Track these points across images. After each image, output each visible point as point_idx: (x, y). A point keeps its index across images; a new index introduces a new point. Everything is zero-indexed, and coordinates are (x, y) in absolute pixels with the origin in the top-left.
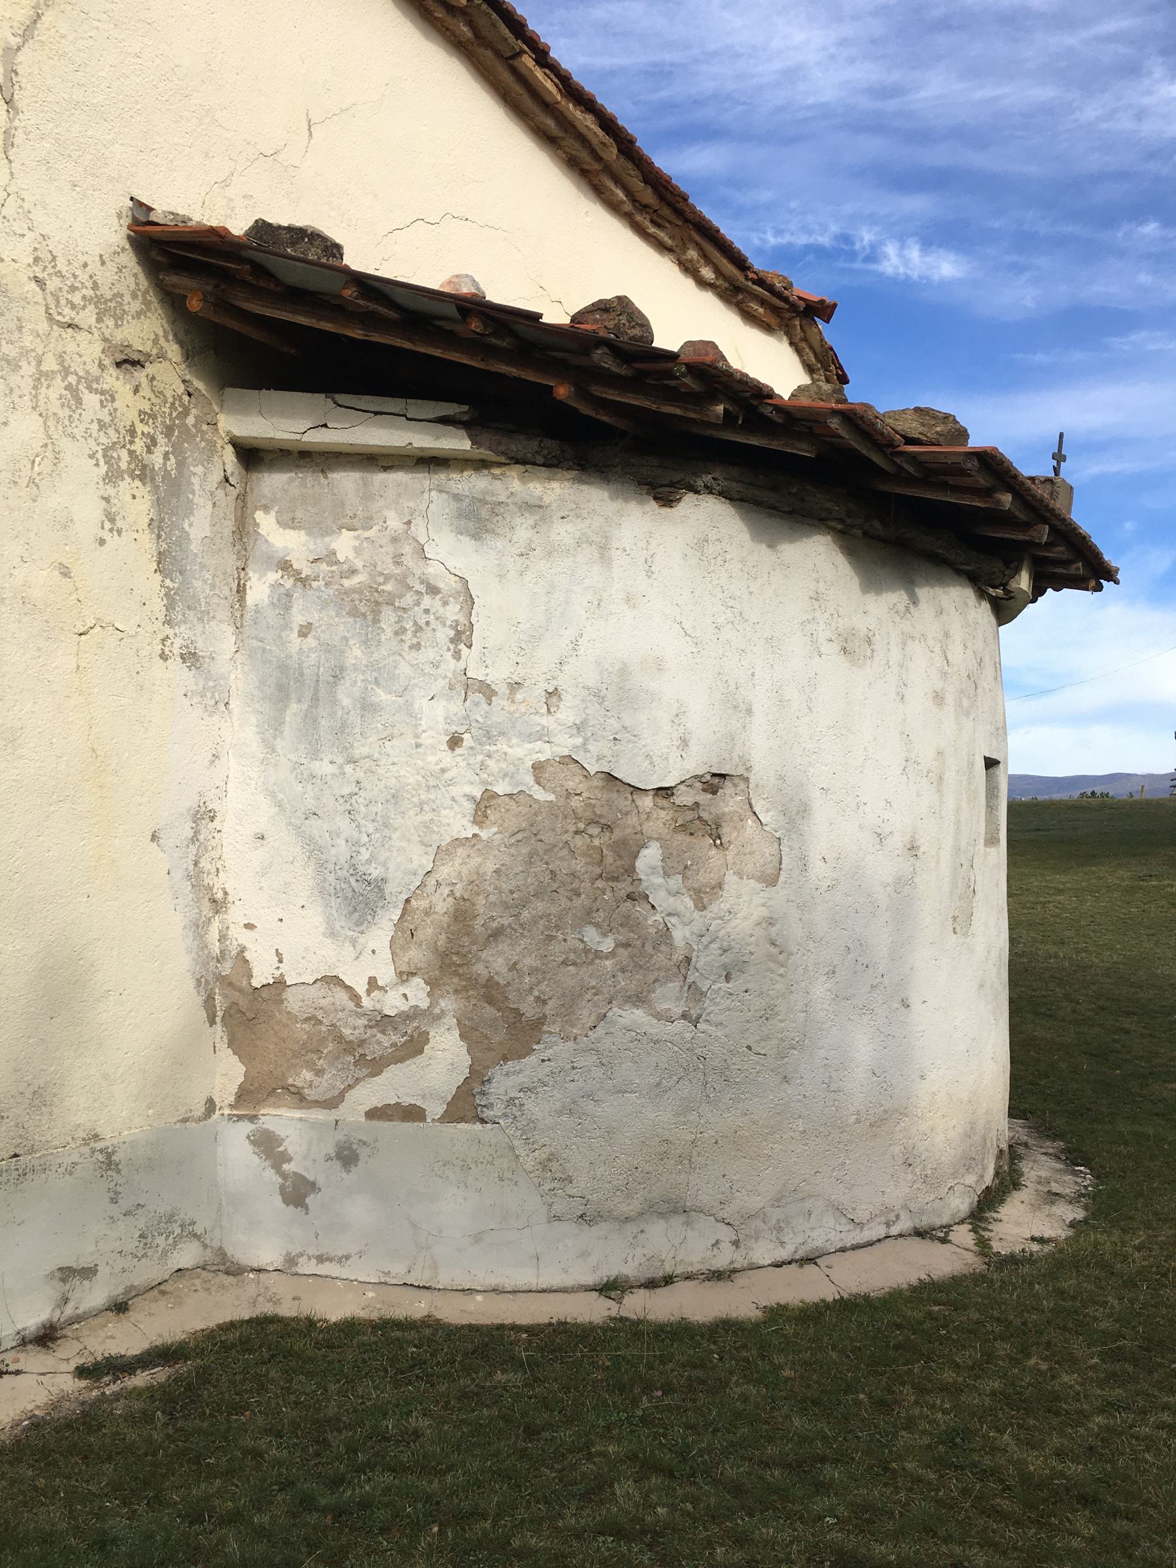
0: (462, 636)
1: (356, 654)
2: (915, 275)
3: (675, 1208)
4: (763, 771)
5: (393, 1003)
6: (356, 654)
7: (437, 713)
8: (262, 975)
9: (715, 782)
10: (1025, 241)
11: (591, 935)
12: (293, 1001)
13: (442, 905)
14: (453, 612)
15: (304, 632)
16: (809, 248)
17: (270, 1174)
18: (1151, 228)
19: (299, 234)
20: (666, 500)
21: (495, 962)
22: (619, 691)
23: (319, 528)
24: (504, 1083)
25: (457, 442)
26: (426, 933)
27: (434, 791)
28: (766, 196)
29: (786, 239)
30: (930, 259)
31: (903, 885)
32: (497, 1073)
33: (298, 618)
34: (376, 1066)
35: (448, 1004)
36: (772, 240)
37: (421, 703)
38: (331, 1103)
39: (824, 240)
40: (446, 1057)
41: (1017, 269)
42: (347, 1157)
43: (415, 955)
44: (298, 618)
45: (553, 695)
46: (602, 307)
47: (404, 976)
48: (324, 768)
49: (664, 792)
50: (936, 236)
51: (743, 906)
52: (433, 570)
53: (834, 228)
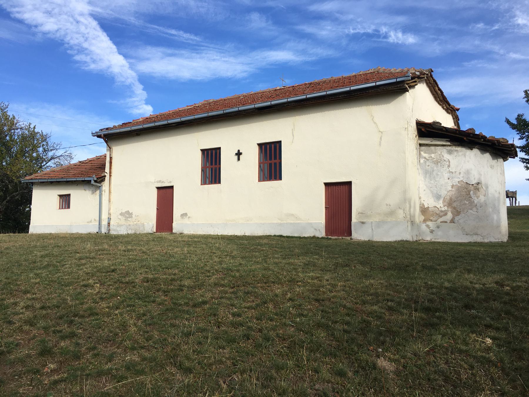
0: (449, 166)
1: (435, 168)
2: (400, 42)
3: (476, 234)
4: (483, 182)
5: (443, 209)
6: (435, 168)
7: (446, 175)
8: (426, 206)
9: (478, 184)
10: (439, 31)
11: (465, 201)
12: (430, 209)
13: (448, 198)
14: (448, 163)
15: (428, 166)
16: (364, 34)
17: (428, 229)
18: (481, 25)
19: (438, 123)
20: (472, 150)
21: (455, 205)
22: (468, 172)
23: (429, 153)
24: (457, 218)
25: (449, 143)
26: (447, 201)
27: (447, 185)
28: (351, 16)
29: (358, 31)
30: (405, 37)
31: (499, 198)
32: (456, 217)
33: (427, 164)
34: (441, 217)
35: (449, 209)
36: (352, 31)
37: (444, 174)
38: (436, 221)
39: (370, 31)
40: (450, 216)
41: (434, 40)
42: (438, 227)
43: (446, 204)
44: (427, 164)
45: (460, 173)
46: (470, 129)
47: (444, 206)
48: (432, 182)
49: (473, 185)
50: (406, 29)
51: (482, 198)
52: (445, 158)
53: (373, 27)
